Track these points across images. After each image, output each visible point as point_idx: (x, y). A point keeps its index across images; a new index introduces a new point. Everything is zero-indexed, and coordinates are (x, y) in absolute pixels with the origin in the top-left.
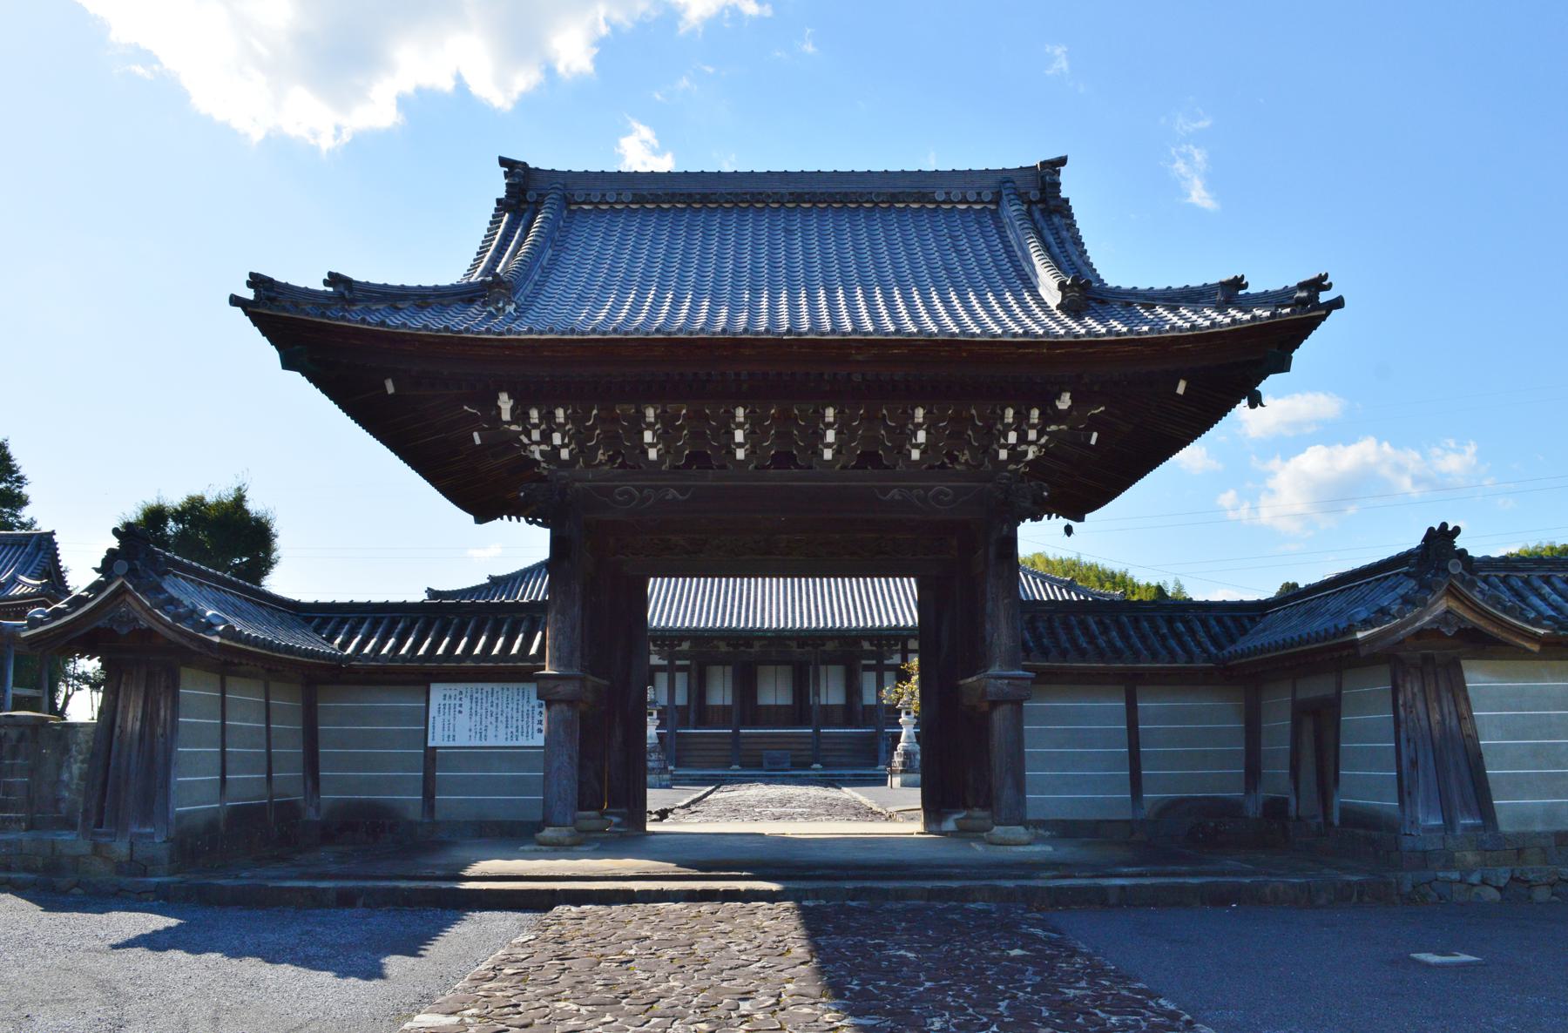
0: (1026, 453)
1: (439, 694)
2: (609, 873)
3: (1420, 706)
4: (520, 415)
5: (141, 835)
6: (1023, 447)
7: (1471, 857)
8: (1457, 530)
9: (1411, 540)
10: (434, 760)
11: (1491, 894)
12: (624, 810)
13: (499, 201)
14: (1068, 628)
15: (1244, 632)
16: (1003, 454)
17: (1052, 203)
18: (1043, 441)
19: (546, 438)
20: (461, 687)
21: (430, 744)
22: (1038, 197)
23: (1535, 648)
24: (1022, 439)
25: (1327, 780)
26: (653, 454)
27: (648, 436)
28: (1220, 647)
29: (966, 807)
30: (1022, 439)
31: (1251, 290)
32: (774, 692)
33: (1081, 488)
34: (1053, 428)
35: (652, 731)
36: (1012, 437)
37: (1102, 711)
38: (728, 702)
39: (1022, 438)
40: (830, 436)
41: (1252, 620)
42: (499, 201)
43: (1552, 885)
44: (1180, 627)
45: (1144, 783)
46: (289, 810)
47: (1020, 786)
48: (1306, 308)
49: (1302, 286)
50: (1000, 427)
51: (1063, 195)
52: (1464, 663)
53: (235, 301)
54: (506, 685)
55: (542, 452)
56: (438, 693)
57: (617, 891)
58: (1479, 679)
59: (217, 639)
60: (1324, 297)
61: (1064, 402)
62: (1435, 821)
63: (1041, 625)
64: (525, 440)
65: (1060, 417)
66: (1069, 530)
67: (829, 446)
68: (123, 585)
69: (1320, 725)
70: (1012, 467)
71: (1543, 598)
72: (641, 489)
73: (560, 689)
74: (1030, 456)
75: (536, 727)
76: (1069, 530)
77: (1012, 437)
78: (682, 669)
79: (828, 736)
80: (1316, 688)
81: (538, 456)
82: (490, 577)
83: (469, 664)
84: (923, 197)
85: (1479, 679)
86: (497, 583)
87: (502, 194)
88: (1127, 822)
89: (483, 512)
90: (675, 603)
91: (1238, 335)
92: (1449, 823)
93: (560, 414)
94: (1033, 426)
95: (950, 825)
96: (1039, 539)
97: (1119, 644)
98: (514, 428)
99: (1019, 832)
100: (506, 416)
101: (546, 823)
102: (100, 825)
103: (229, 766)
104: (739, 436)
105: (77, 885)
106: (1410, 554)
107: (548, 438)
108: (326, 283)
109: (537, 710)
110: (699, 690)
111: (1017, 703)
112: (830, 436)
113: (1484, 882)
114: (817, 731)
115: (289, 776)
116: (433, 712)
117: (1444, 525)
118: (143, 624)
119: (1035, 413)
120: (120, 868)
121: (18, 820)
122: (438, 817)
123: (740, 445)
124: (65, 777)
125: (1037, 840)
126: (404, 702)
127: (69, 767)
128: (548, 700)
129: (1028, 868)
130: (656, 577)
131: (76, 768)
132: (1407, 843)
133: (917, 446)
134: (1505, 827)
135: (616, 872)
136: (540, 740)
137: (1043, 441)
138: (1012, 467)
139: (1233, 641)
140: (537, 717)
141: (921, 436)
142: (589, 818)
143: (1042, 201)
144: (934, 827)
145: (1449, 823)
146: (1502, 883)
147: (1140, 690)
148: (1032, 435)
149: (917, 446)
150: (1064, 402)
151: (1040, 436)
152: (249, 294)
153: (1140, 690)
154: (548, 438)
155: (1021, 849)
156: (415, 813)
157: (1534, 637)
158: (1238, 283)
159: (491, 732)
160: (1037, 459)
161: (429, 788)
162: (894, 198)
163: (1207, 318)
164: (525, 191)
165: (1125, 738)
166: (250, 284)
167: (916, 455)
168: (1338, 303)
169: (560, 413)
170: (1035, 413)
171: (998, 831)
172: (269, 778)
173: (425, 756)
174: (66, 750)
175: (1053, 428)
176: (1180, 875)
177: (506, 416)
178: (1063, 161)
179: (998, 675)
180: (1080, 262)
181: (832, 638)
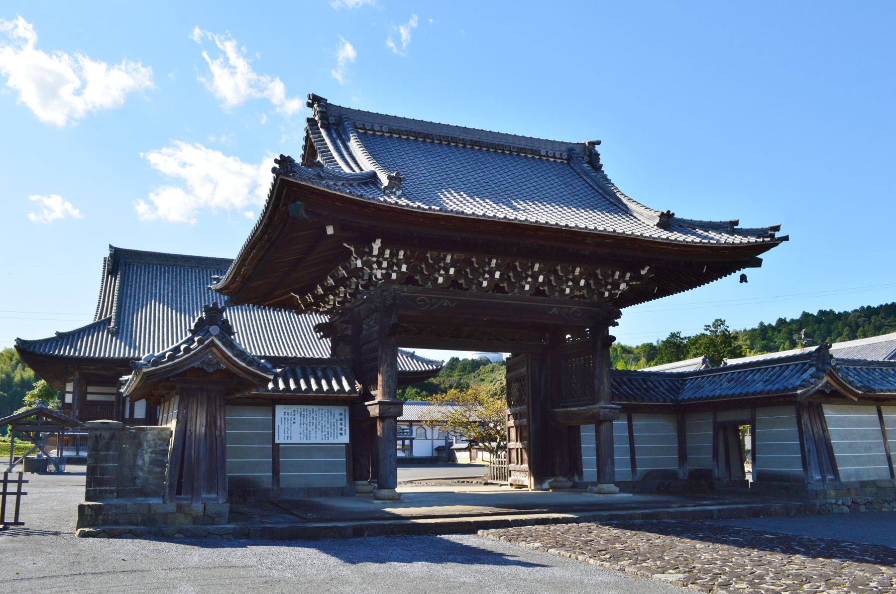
2: (439, 514)
3: (809, 425)
5: (209, 499)
7: (832, 493)
10: (278, 451)
11: (846, 509)
20: (295, 407)
21: (277, 441)
23: (856, 399)
29: (553, 475)
48: (769, 238)
52: (823, 406)
54: (321, 407)
57: (501, 521)
58: (830, 413)
60: (778, 235)
62: (819, 477)
68: (212, 341)
69: (728, 436)
72: (430, 299)
73: (392, 410)
75: (339, 432)
82: (58, 333)
83: (311, 394)
84: (534, 152)
85: (830, 413)
86: (63, 338)
88: (631, 482)
91: (734, 248)
92: (824, 479)
95: (546, 485)
102: (179, 492)
105: (179, 532)
113: (843, 504)
116: (278, 422)
118: (223, 366)
120: (195, 520)
121: (112, 492)
122: (281, 486)
124: (140, 462)
126: (261, 416)
127: (142, 456)
131: (147, 457)
132: (810, 487)
134: (843, 480)
135: (432, 514)
136: (345, 439)
140: (339, 426)
144: (539, 487)
145: (824, 479)
146: (849, 503)
147: (634, 416)
153: (634, 416)
156: (268, 484)
157: (856, 395)
158: (736, 223)
159: (313, 435)
161: (276, 468)
162: (520, 150)
163: (724, 238)
165: (628, 439)
168: (786, 238)
173: (273, 449)
174: (140, 445)
176: (705, 505)
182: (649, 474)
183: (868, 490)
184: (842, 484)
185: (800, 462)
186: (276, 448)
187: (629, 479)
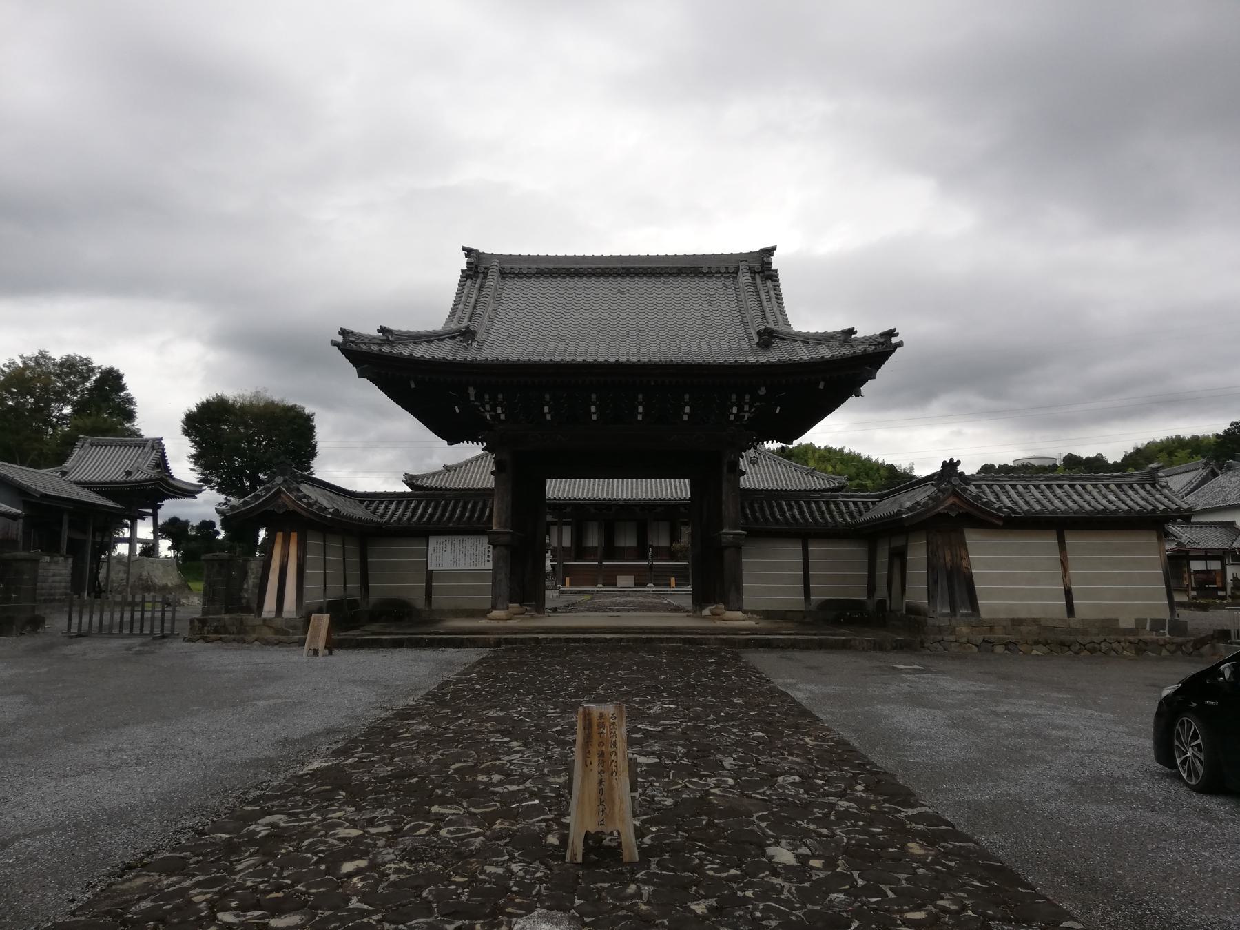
4: (479, 397)
8: (959, 462)
9: (937, 468)
13: (463, 271)
16: (732, 417)
19: (493, 409)
23: (1001, 523)
26: (549, 417)
31: (858, 335)
32: (627, 541)
35: (548, 564)
36: (735, 410)
37: (789, 555)
38: (596, 545)
39: (740, 409)
40: (640, 409)
42: (463, 271)
43: (1006, 645)
44: (833, 507)
45: (812, 591)
46: (353, 603)
47: (739, 590)
49: (882, 335)
51: (774, 267)
53: (334, 343)
56: (433, 541)
60: (894, 340)
61: (762, 391)
62: (947, 611)
71: (1009, 497)
77: (735, 410)
78: (566, 524)
80: (898, 542)
89: (452, 439)
90: (558, 489)
97: (798, 516)
99: (739, 614)
100: (472, 398)
101: (494, 608)
106: (934, 475)
110: (578, 537)
111: (738, 548)
112: (640, 409)
115: (354, 586)
117: (952, 460)
119: (747, 397)
125: (750, 619)
126: (417, 546)
128: (494, 544)
129: (737, 631)
132: (930, 621)
134: (984, 614)
136: (489, 566)
143: (762, 272)
148: (746, 408)
150: (762, 391)
151: (750, 408)
152: (340, 339)
158: (851, 331)
159: (462, 562)
164: (478, 267)
168: (900, 344)
169: (500, 396)
170: (747, 397)
171: (729, 614)
177: (472, 398)
178: (774, 248)
180: (777, 312)
181: (661, 505)
182: (826, 605)
183: (1024, 629)
184: (984, 621)
185: (1074, 594)
186: (430, 575)
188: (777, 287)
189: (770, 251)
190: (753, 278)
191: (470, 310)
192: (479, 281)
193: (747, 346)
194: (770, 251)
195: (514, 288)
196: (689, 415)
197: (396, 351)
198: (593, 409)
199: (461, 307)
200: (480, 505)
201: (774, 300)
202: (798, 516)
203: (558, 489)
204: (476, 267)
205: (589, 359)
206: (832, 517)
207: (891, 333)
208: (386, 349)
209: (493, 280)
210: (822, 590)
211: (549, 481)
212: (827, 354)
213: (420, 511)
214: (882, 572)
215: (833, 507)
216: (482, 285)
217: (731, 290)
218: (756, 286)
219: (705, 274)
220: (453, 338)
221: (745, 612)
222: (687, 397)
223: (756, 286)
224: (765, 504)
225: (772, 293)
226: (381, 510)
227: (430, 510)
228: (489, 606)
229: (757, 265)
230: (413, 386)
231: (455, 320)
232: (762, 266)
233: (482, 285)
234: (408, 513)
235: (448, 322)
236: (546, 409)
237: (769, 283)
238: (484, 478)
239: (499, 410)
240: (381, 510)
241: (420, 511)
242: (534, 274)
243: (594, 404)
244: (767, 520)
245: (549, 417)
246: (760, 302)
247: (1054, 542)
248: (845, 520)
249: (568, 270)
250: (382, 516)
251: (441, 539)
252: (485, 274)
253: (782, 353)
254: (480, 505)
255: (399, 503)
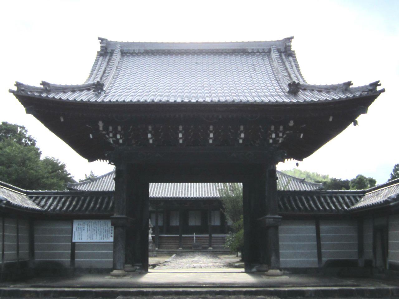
0: (279, 141)
1: (76, 225)
4: (106, 128)
6: (278, 139)
12: (141, 264)
13: (98, 52)
14: (295, 201)
15: (357, 201)
16: (271, 141)
17: (289, 52)
18: (285, 136)
19: (115, 136)
21: (73, 241)
22: (285, 50)
24: (276, 137)
25: (385, 254)
26: (151, 141)
27: (149, 136)
28: (348, 206)
30: (276, 137)
32: (194, 222)
33: (301, 152)
34: (288, 132)
35: (150, 236)
36: (274, 136)
37: (308, 230)
38: (178, 224)
39: (277, 136)
40: (211, 135)
41: (360, 197)
42: (98, 52)
44: (334, 199)
47: (278, 256)
48: (371, 94)
50: (269, 132)
51: (292, 49)
53: (11, 91)
55: (113, 141)
59: (4, 206)
60: (379, 88)
61: (291, 123)
63: (286, 200)
64: (107, 136)
65: (290, 128)
66: (297, 164)
67: (211, 138)
70: (274, 145)
74: (280, 141)
76: (297, 164)
77: (274, 136)
79: (214, 237)
81: (111, 142)
83: (87, 213)
87: (99, 50)
89: (91, 158)
90: (158, 190)
93: (119, 128)
94: (281, 132)
96: (286, 167)
97: (313, 206)
98: (104, 132)
100: (101, 129)
101: (114, 268)
103: (5, 249)
104: (180, 135)
107: (116, 138)
108: (41, 84)
109: (111, 229)
110: (167, 221)
111: (276, 228)
112: (211, 135)
114: (210, 235)
115: (24, 252)
116: (74, 229)
119: (281, 128)
123: (181, 138)
125: (284, 274)
126: (67, 227)
130: (153, 182)
133: (241, 138)
136: (112, 240)
137: (285, 136)
138: (274, 145)
139: (353, 204)
141: (242, 135)
142: (128, 267)
148: (281, 135)
149: (241, 138)
150: (291, 123)
151: (283, 135)
152: (15, 89)
154: (116, 138)
155: (278, 278)
158: (349, 83)
159: (95, 237)
160: (282, 143)
164: (107, 50)
165: (315, 239)
166: (16, 85)
167: (241, 141)
168: (383, 91)
170: (281, 128)
171: (271, 271)
172: (18, 253)
175: (288, 132)
177: (101, 129)
178: (292, 38)
179: (270, 218)
182: (333, 264)
186: (74, 245)
187: (316, 266)
188: (295, 61)
189: (289, 39)
190: (281, 56)
191: (101, 73)
192: (108, 58)
193: (281, 94)
194: (289, 39)
195: (130, 63)
196: (244, 140)
197: (51, 96)
198: (180, 135)
199: (95, 72)
200: (106, 200)
201: (294, 68)
202: (313, 206)
203: (158, 190)
204: (106, 49)
205: (179, 100)
206: (335, 206)
207: (376, 84)
208: (44, 95)
209: (117, 57)
210: (328, 255)
211: (151, 184)
212: (336, 97)
213: (67, 203)
214: (369, 241)
215: (334, 199)
216: (109, 60)
217: (267, 62)
218: (282, 60)
219: (249, 53)
220: (89, 90)
221: (281, 270)
222: (242, 128)
223: (282, 60)
224: (291, 198)
225: (293, 64)
226: (43, 203)
227: (74, 203)
228: (111, 266)
229: (283, 49)
230: (62, 120)
231: (92, 79)
232: (285, 48)
233: (109, 60)
234: (60, 205)
235: (89, 79)
236: (149, 136)
237: (291, 59)
238: (110, 185)
239: (118, 136)
240: (43, 203)
241: (67, 203)
242: (142, 54)
243: (181, 132)
244: (293, 209)
245: (151, 141)
246: (286, 69)
247: (313, 227)
248: (343, 208)
249: (164, 50)
250: (43, 207)
251: (81, 222)
252: (112, 53)
253: (304, 97)
254: (106, 200)
255: (55, 199)
